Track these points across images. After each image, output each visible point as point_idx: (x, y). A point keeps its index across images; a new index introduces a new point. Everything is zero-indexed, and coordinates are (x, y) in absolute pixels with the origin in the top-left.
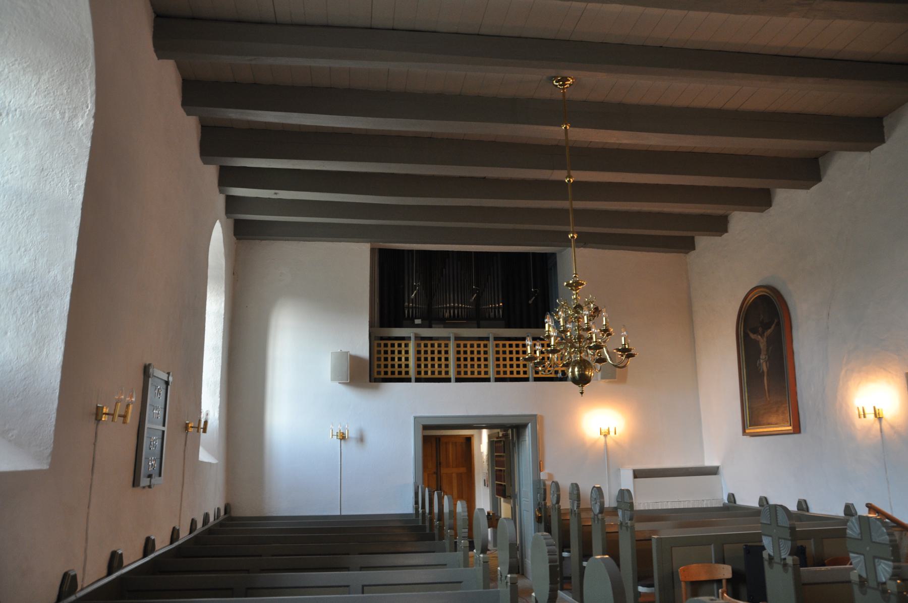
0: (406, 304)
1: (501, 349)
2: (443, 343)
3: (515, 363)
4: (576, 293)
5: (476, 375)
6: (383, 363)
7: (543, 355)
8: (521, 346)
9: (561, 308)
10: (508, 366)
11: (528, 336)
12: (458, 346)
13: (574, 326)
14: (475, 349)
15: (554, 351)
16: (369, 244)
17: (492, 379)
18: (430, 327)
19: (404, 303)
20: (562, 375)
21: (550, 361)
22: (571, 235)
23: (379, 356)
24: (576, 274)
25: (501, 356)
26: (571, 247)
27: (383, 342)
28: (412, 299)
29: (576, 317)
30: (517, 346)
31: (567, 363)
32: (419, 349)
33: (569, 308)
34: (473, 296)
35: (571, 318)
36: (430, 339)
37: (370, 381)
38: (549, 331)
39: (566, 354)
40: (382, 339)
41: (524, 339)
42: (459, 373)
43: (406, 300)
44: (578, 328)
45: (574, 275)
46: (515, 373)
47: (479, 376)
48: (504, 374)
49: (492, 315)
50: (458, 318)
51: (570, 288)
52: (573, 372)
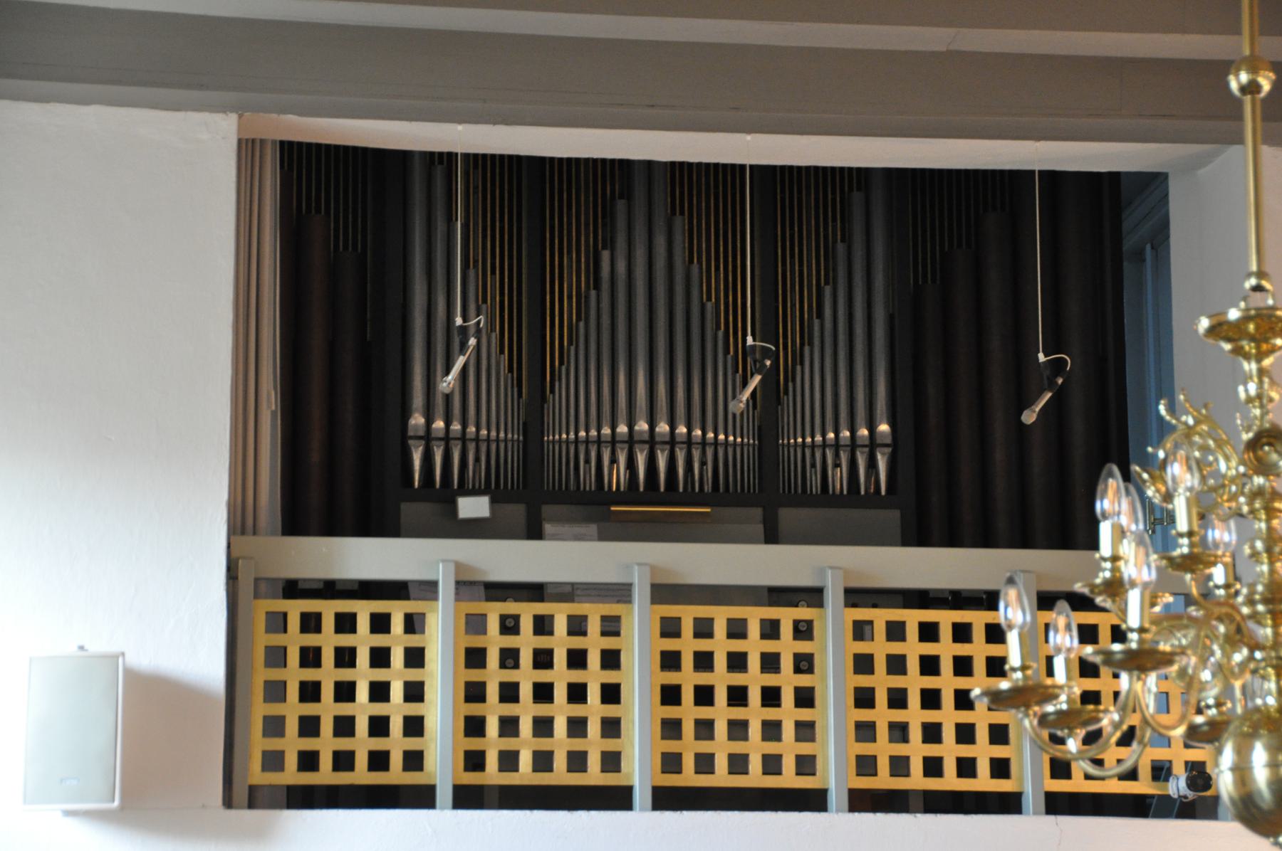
0: (417, 420)
1: (880, 648)
2: (594, 613)
3: (948, 716)
4: (1261, 372)
5: (755, 778)
6: (293, 709)
7: (1091, 684)
8: (979, 634)
9: (1177, 446)
10: (916, 733)
11: (1011, 581)
12: (670, 629)
13: (1246, 536)
14: (754, 646)
15: (1141, 661)
16: (233, 117)
17: (833, 799)
18: (534, 532)
19: (406, 414)
20: (1192, 784)
21: (1123, 710)
22: (1244, 77)
23: (276, 674)
24: (1261, 274)
25: (881, 682)
26: (1240, 140)
27: (295, 609)
28: (448, 398)
29: (1258, 493)
30: (962, 633)
31: (1212, 723)
32: (476, 642)
33: (1220, 444)
34: (745, 384)
35: (1233, 497)
36: (535, 591)
37: (228, 803)
38: (1115, 558)
39: (1206, 675)
40: (292, 589)
41: (989, 600)
42: (671, 763)
43: (418, 400)
44: (1269, 550)
45: (1253, 281)
46: (950, 767)
47: (771, 782)
48: (961, 774)
49: (839, 478)
50: (672, 494)
51: (1227, 347)
52: (1242, 771)
